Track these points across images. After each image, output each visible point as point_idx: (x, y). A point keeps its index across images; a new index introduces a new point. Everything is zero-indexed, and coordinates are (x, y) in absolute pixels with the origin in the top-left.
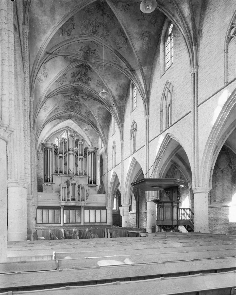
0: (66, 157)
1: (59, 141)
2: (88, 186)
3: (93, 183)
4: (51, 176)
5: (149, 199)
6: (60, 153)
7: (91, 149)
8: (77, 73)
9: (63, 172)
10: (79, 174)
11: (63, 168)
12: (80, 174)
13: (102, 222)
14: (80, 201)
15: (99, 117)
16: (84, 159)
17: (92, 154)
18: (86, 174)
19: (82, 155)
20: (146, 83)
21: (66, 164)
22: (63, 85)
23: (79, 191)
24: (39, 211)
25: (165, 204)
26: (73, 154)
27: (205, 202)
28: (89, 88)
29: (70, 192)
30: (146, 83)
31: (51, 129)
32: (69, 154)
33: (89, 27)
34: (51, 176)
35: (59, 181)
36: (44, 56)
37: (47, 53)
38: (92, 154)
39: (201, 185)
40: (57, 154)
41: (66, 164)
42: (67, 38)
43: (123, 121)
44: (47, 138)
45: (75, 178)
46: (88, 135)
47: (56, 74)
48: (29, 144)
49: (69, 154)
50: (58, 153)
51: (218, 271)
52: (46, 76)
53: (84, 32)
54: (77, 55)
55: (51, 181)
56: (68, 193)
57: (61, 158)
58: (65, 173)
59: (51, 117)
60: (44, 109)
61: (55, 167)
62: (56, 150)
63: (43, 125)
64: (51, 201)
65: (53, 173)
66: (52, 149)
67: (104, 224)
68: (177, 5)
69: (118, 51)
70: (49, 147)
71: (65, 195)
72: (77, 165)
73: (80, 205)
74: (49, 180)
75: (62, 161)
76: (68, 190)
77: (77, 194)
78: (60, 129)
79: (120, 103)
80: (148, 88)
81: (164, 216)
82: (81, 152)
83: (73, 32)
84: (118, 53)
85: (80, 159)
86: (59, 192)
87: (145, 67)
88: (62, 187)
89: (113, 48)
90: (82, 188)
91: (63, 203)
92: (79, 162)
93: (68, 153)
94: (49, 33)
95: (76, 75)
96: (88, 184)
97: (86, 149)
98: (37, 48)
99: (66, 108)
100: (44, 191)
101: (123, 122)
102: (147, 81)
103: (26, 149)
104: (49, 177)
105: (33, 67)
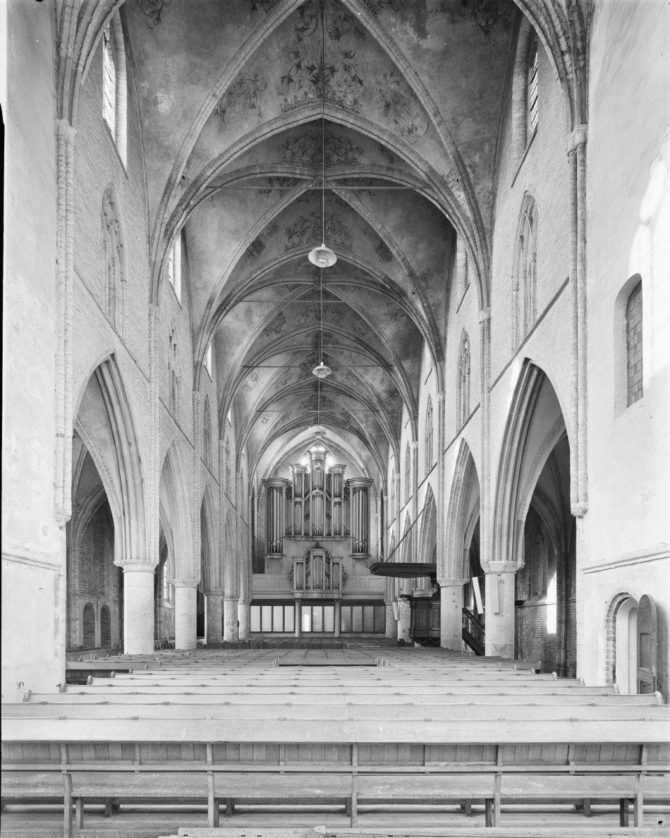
0: (307, 502)
1: (295, 472)
2: (351, 558)
3: (362, 552)
4: (278, 542)
5: (416, 591)
6: (295, 496)
7: (359, 483)
8: (310, 363)
9: (301, 531)
10: (333, 535)
11: (300, 523)
12: (335, 534)
13: (365, 630)
14: (329, 588)
15: (367, 421)
16: (343, 505)
17: (361, 492)
18: (347, 533)
19: (340, 496)
20: (410, 387)
21: (307, 516)
22: (287, 385)
23: (329, 571)
24: (255, 610)
25: (419, 602)
26: (322, 496)
28: (335, 383)
29: (312, 572)
30: (410, 387)
31: (283, 446)
32: (314, 497)
33: (309, 314)
35: (293, 550)
36: (242, 370)
37: (244, 367)
39: (446, 575)
40: (291, 496)
41: (307, 516)
42: (275, 337)
43: (400, 436)
44: (278, 463)
45: (326, 542)
46: (359, 449)
47: (271, 375)
49: (314, 497)
51: (166, 634)
52: (256, 380)
53: (302, 321)
54: (301, 344)
55: (280, 550)
56: (308, 574)
57: (298, 506)
58: (307, 534)
59: (276, 430)
60: (262, 419)
61: (287, 523)
63: (263, 448)
64: (276, 589)
65: (284, 535)
66: (281, 489)
67: (329, 636)
68: (411, 304)
69: (361, 338)
72: (329, 516)
73: (330, 596)
74: (275, 549)
75: (300, 511)
76: (307, 568)
78: (303, 442)
79: (390, 404)
81: (417, 622)
82: (337, 490)
83: (284, 327)
84: (363, 342)
85: (335, 503)
86: (291, 573)
87: (407, 361)
88: (295, 565)
89: (353, 336)
90: (334, 564)
91: (298, 595)
92: (334, 511)
93: (310, 495)
94: (245, 342)
96: (351, 553)
97: (348, 482)
98: (228, 365)
99: (305, 410)
100: (266, 570)
101: (400, 439)
102: (413, 383)
103: (196, 540)
104: (275, 544)
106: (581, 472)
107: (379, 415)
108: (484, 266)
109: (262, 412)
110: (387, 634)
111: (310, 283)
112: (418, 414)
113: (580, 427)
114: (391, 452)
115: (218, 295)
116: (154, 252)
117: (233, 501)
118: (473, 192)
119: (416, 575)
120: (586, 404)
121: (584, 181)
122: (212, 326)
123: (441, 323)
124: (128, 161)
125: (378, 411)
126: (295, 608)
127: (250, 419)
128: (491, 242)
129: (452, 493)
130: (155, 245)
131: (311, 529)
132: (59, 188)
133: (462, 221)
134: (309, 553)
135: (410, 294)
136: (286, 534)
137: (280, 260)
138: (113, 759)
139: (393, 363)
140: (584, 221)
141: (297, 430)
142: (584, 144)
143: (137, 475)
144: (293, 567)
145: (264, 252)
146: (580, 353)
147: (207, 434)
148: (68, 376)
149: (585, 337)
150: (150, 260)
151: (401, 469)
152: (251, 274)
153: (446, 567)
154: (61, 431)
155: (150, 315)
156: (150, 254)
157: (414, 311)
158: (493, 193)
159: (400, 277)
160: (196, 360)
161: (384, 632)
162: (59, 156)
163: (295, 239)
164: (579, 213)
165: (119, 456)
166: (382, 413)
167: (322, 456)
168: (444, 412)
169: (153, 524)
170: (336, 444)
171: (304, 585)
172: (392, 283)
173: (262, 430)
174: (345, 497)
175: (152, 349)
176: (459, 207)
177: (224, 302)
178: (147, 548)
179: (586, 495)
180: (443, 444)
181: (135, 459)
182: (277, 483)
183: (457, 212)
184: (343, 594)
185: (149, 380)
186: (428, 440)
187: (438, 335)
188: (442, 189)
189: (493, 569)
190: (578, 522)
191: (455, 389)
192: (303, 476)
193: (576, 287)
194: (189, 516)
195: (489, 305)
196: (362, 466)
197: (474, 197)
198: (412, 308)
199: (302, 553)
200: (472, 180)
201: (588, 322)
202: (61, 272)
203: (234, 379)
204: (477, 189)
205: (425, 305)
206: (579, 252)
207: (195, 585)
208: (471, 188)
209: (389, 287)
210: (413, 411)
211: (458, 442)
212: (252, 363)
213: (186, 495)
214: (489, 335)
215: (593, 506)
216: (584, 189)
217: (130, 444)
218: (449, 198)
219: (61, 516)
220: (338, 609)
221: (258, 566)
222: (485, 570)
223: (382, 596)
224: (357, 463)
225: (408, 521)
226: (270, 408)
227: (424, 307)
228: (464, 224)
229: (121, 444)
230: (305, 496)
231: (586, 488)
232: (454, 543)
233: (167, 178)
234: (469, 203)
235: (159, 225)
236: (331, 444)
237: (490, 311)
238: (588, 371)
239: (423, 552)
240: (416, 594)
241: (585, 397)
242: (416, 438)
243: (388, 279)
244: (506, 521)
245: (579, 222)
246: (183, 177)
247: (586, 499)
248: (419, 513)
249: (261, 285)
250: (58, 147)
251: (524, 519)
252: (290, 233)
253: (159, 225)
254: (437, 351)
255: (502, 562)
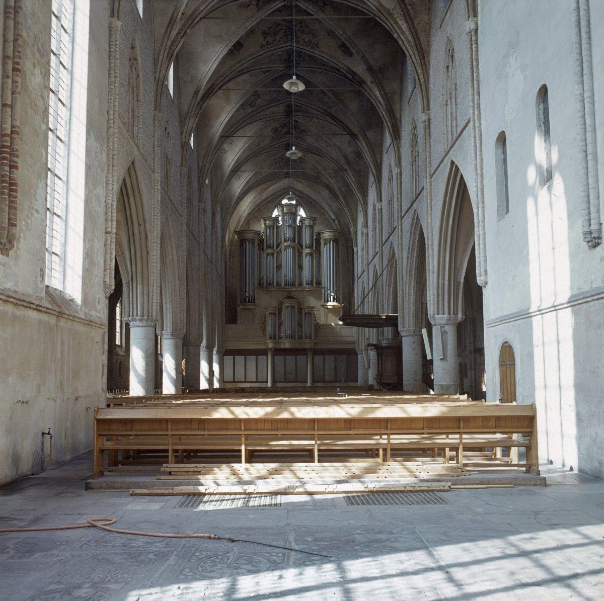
4: (251, 292)
6: (268, 247)
14: (302, 338)
20: (374, 153)
22: (260, 147)
27: (29, 403)
30: (374, 153)
34: (251, 292)
38: (330, 243)
39: (407, 326)
48: (186, 290)
50: (265, 248)
52: (231, 144)
55: (253, 301)
57: (270, 257)
58: (279, 284)
62: (261, 241)
65: (257, 285)
66: (253, 241)
70: (248, 238)
71: (274, 328)
77: (297, 326)
80: (378, 161)
88: (268, 315)
95: (280, 129)
100: (239, 322)
101: (367, 196)
103: (182, 297)
104: (247, 294)
105: (203, 162)
106: (482, 255)
107: (347, 173)
108: (424, 78)
109: (236, 172)
110: (359, 383)
111: (283, 69)
112: (381, 177)
113: (480, 223)
114: (360, 208)
115: (203, 87)
116: (158, 71)
117: (209, 256)
118: (413, 23)
119: (383, 326)
120: (483, 207)
121: (477, 55)
122: (197, 112)
123: (396, 107)
124: (144, 9)
125: (346, 170)
126: (268, 357)
127: (225, 179)
128: (429, 61)
129: (408, 254)
130: (159, 65)
131: (283, 279)
132: (110, 63)
133: (406, 43)
134: (281, 303)
135: (369, 83)
136: (259, 285)
137: (257, 55)
138: (194, 430)
139: (358, 133)
140: (478, 81)
141: (269, 183)
142: (476, 30)
143: (144, 248)
144: (265, 317)
145: (242, 50)
146: (479, 171)
147: (190, 200)
148: (114, 190)
149: (482, 160)
150: (155, 77)
151: (369, 224)
152: (231, 67)
153: (406, 319)
154: (109, 229)
155: (154, 120)
156: (155, 72)
157: (373, 97)
158: (429, 24)
159: (360, 69)
160: (183, 140)
161: (357, 381)
162: (110, 41)
163: (269, 39)
164: (475, 75)
165: (131, 234)
166: (349, 171)
167: (294, 209)
168: (401, 183)
169: (155, 287)
170: (306, 195)
171: (277, 335)
172: (354, 74)
173: (238, 186)
174: (316, 248)
175: (156, 147)
176: (403, 32)
177: (208, 91)
178: (150, 307)
179: (486, 271)
180: (401, 210)
181: (143, 235)
182: (249, 235)
183: (401, 36)
184: (315, 343)
185: (153, 172)
186: (390, 202)
187: (394, 117)
188: (389, 18)
189: (438, 322)
190: (484, 291)
191: (409, 167)
192: (275, 228)
193: (474, 125)
194: (177, 275)
195: (429, 109)
196: (333, 217)
197: (414, 27)
198: (371, 94)
199: (275, 303)
200: (412, 15)
201: (483, 150)
202: (111, 119)
203: (213, 147)
204: (416, 22)
205: (382, 93)
206: (476, 102)
207: (181, 336)
208: (412, 21)
209: (351, 77)
210: (377, 175)
211: (447, 162)
212: (229, 133)
213: (175, 257)
214: (430, 132)
215: (491, 279)
216: (477, 59)
217: (140, 225)
218: (395, 26)
219: (108, 290)
220: (310, 359)
221: (232, 317)
222: (432, 322)
223: (353, 345)
224: (328, 214)
225: (375, 272)
226: (243, 169)
227: (381, 95)
228: (407, 46)
229: (132, 225)
230: (277, 247)
231: (485, 266)
232: (412, 298)
233: (170, 15)
234: (410, 31)
235: (162, 51)
236: (301, 195)
237: (430, 114)
238: (484, 185)
239: (388, 304)
240: (384, 343)
241: (483, 202)
242: (380, 199)
243: (350, 70)
244: (446, 283)
245: (475, 82)
246: (183, 14)
247: (486, 274)
248: (384, 267)
249: (241, 73)
250: (110, 35)
251: (462, 281)
252: (265, 34)
253: (162, 51)
254: (394, 131)
255: (445, 316)
